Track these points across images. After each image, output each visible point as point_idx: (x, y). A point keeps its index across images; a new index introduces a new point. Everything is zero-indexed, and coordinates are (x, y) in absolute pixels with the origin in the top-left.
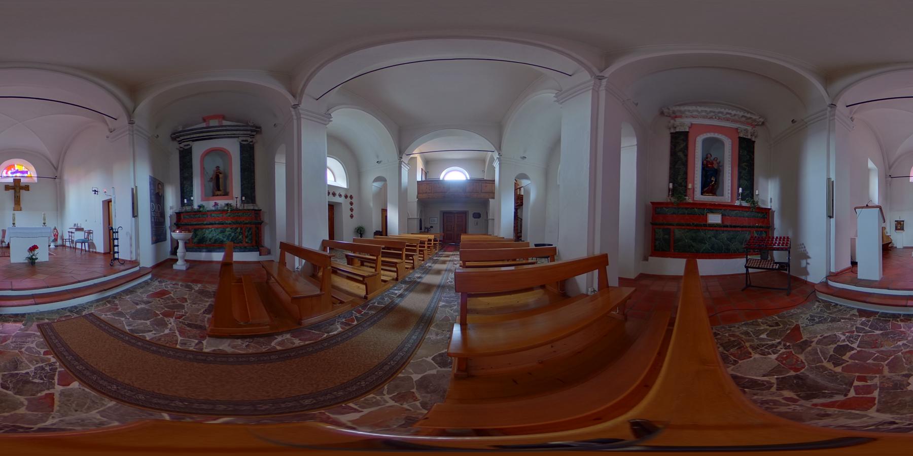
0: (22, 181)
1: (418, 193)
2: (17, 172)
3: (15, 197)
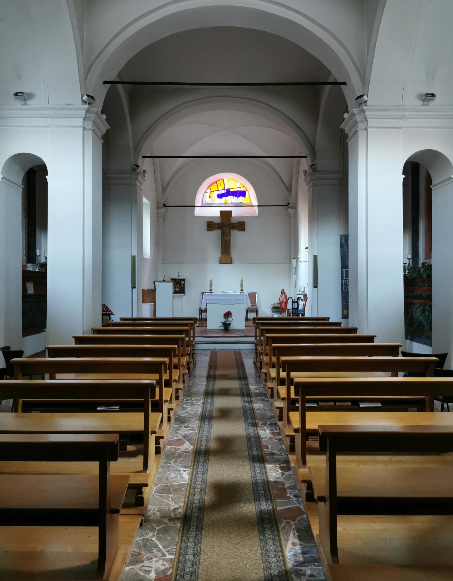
0: (233, 215)
2: (228, 193)
3: (222, 242)
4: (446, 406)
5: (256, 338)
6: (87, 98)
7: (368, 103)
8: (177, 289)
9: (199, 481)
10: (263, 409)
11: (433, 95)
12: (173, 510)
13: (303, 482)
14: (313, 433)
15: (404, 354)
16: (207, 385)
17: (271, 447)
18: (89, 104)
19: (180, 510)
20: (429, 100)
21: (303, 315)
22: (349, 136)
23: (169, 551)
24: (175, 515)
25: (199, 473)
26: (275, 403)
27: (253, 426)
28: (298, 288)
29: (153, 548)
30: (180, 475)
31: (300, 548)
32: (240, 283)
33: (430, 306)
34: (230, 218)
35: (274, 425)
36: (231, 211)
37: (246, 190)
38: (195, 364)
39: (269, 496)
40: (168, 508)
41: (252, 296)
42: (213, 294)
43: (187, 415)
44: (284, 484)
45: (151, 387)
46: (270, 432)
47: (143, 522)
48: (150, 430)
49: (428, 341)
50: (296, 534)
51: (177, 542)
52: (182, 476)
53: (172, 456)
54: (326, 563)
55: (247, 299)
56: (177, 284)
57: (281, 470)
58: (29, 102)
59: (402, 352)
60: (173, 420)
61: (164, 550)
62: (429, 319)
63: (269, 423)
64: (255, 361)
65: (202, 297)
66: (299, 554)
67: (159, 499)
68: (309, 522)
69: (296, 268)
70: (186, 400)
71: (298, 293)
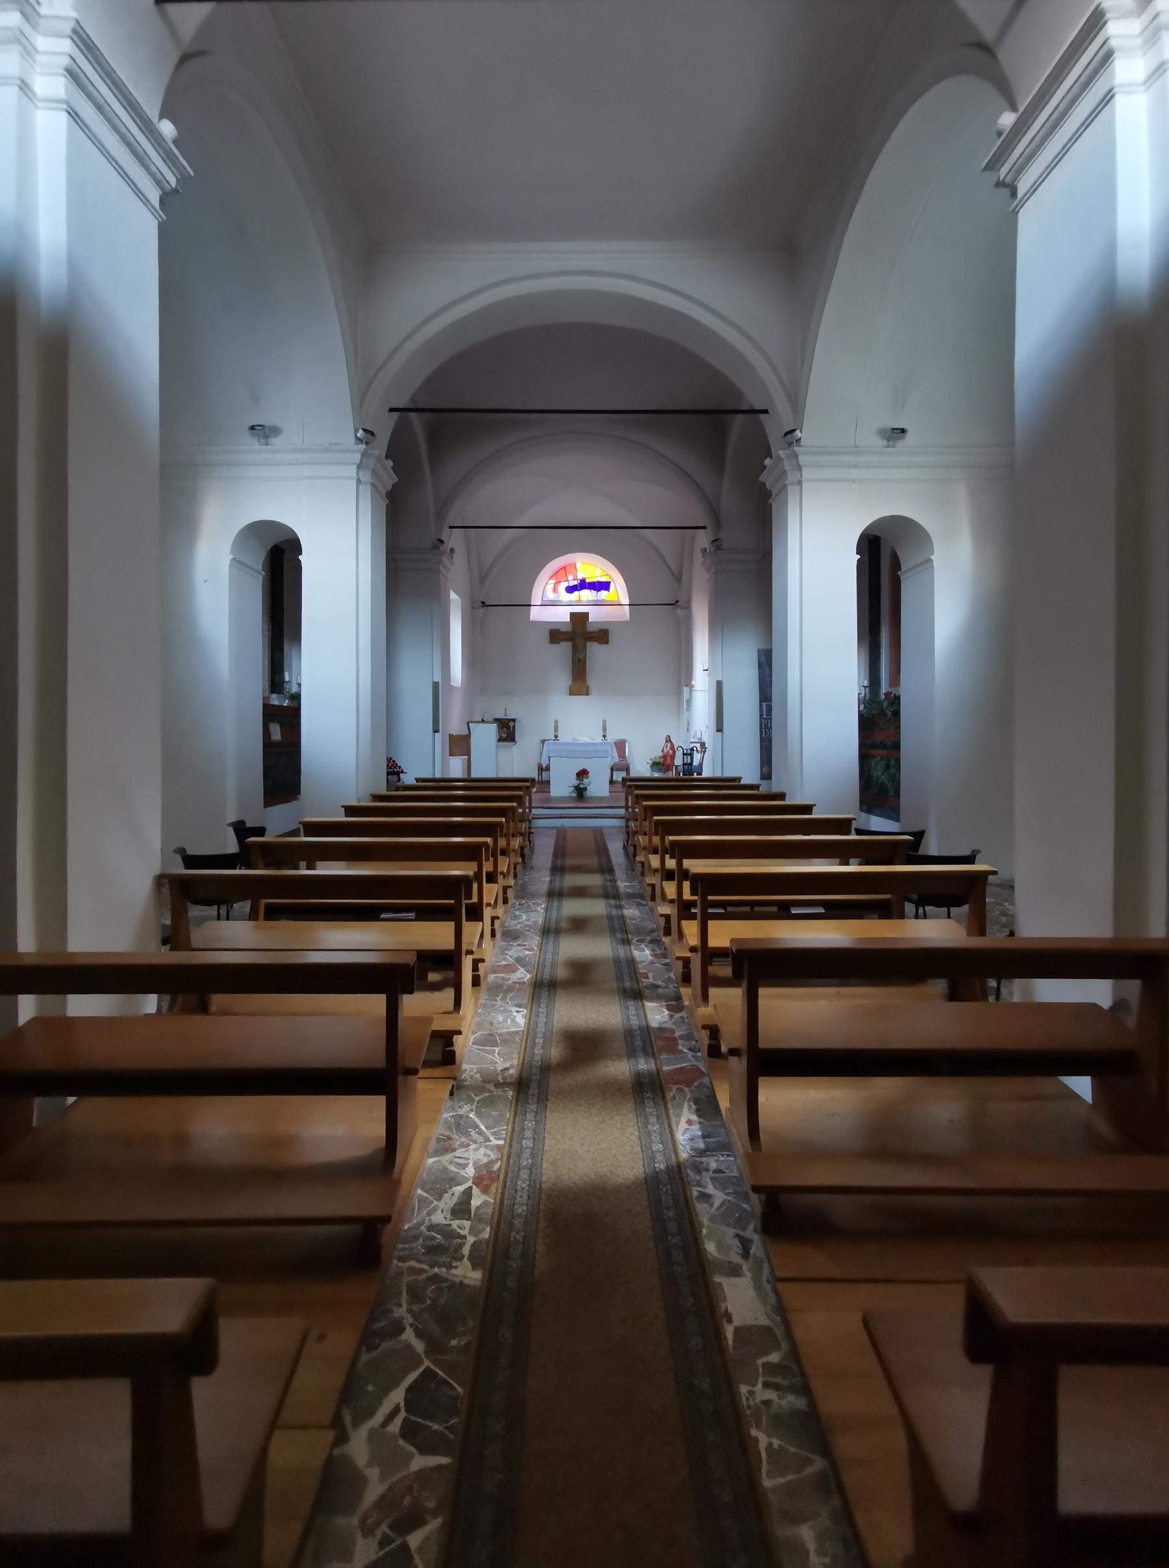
2: (583, 585)
4: (922, 911)
5: (627, 810)
6: (364, 433)
7: (802, 443)
8: (503, 735)
9: (541, 1027)
10: (639, 917)
11: (903, 431)
12: (501, 1071)
13: (704, 1027)
14: (721, 953)
15: (859, 832)
16: (551, 882)
17: (653, 977)
18: (367, 443)
19: (511, 1071)
20: (898, 439)
21: (700, 773)
22: (773, 494)
23: (494, 1134)
24: (504, 1079)
25: (540, 1015)
26: (659, 908)
27: (623, 944)
28: (692, 732)
29: (470, 1130)
30: (511, 1018)
31: (700, 1128)
32: (601, 725)
33: (898, 761)
34: (586, 624)
35: (656, 942)
36: (588, 613)
37: (610, 580)
38: (532, 850)
39: (650, 1050)
40: (493, 1068)
41: (620, 746)
42: (560, 741)
43: (521, 927)
44: (673, 1031)
45: (465, 881)
46: (651, 952)
47: (455, 1089)
48: (464, 948)
49: (893, 813)
50: (694, 1107)
51: (508, 1119)
52: (513, 1020)
53: (497, 989)
54: (741, 1151)
55: (612, 749)
56: (502, 728)
57: (668, 1010)
58: (273, 440)
59: (855, 829)
60: (498, 935)
61: (488, 1133)
62: (896, 780)
63: (648, 938)
64: (626, 844)
65: (543, 746)
66: (698, 1137)
67: (479, 1054)
68: (713, 1088)
69: (689, 702)
70: (519, 905)
71: (692, 740)
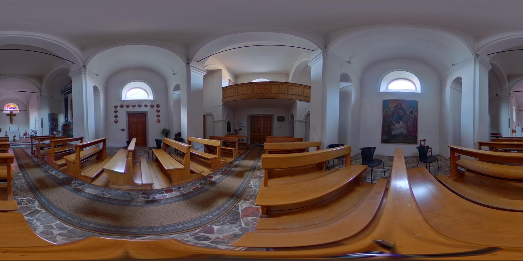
1: (223, 97)
2: (11, 108)
52: (254, 182)
